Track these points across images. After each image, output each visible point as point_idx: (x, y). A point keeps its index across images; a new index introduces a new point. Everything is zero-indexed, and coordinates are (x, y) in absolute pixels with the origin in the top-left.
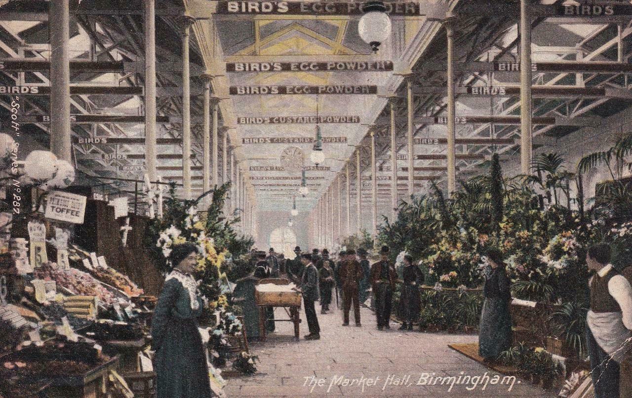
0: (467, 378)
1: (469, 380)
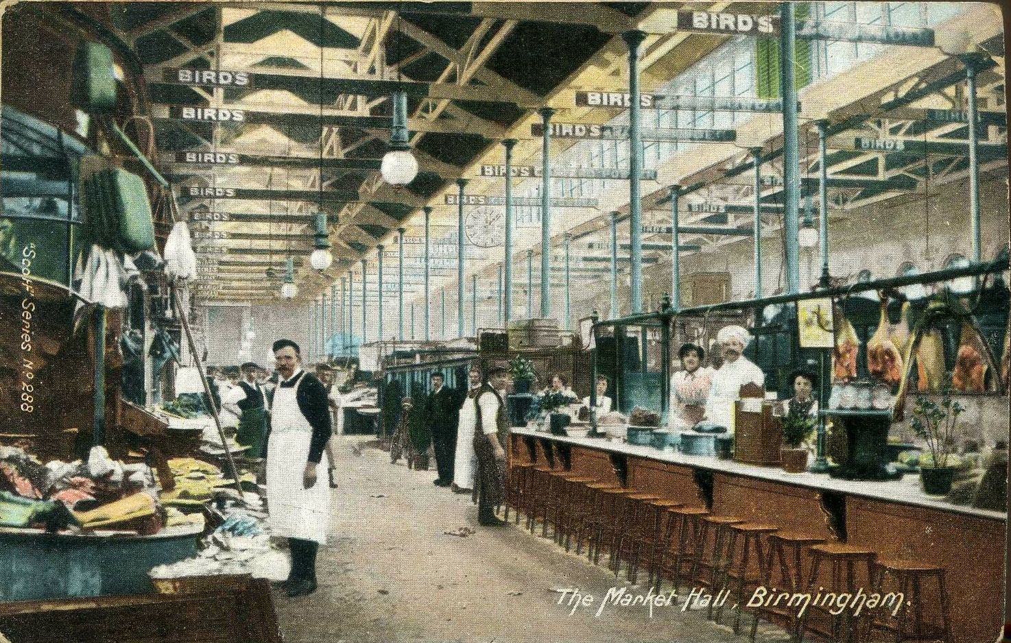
0: (830, 598)
1: (833, 601)
